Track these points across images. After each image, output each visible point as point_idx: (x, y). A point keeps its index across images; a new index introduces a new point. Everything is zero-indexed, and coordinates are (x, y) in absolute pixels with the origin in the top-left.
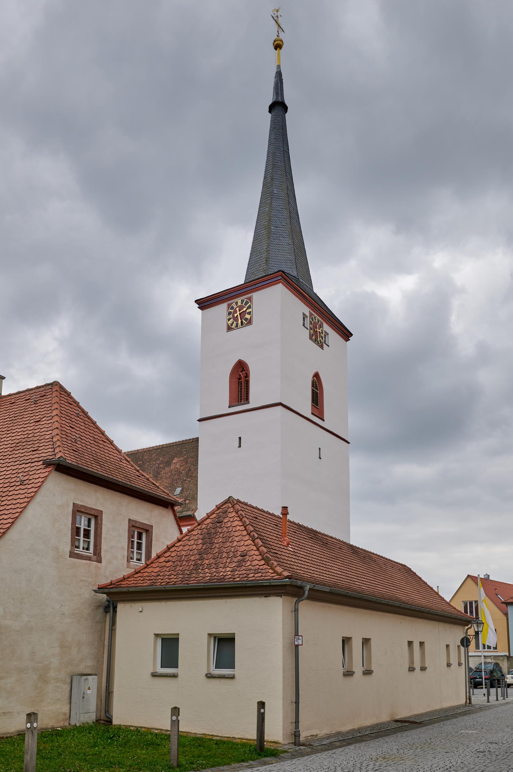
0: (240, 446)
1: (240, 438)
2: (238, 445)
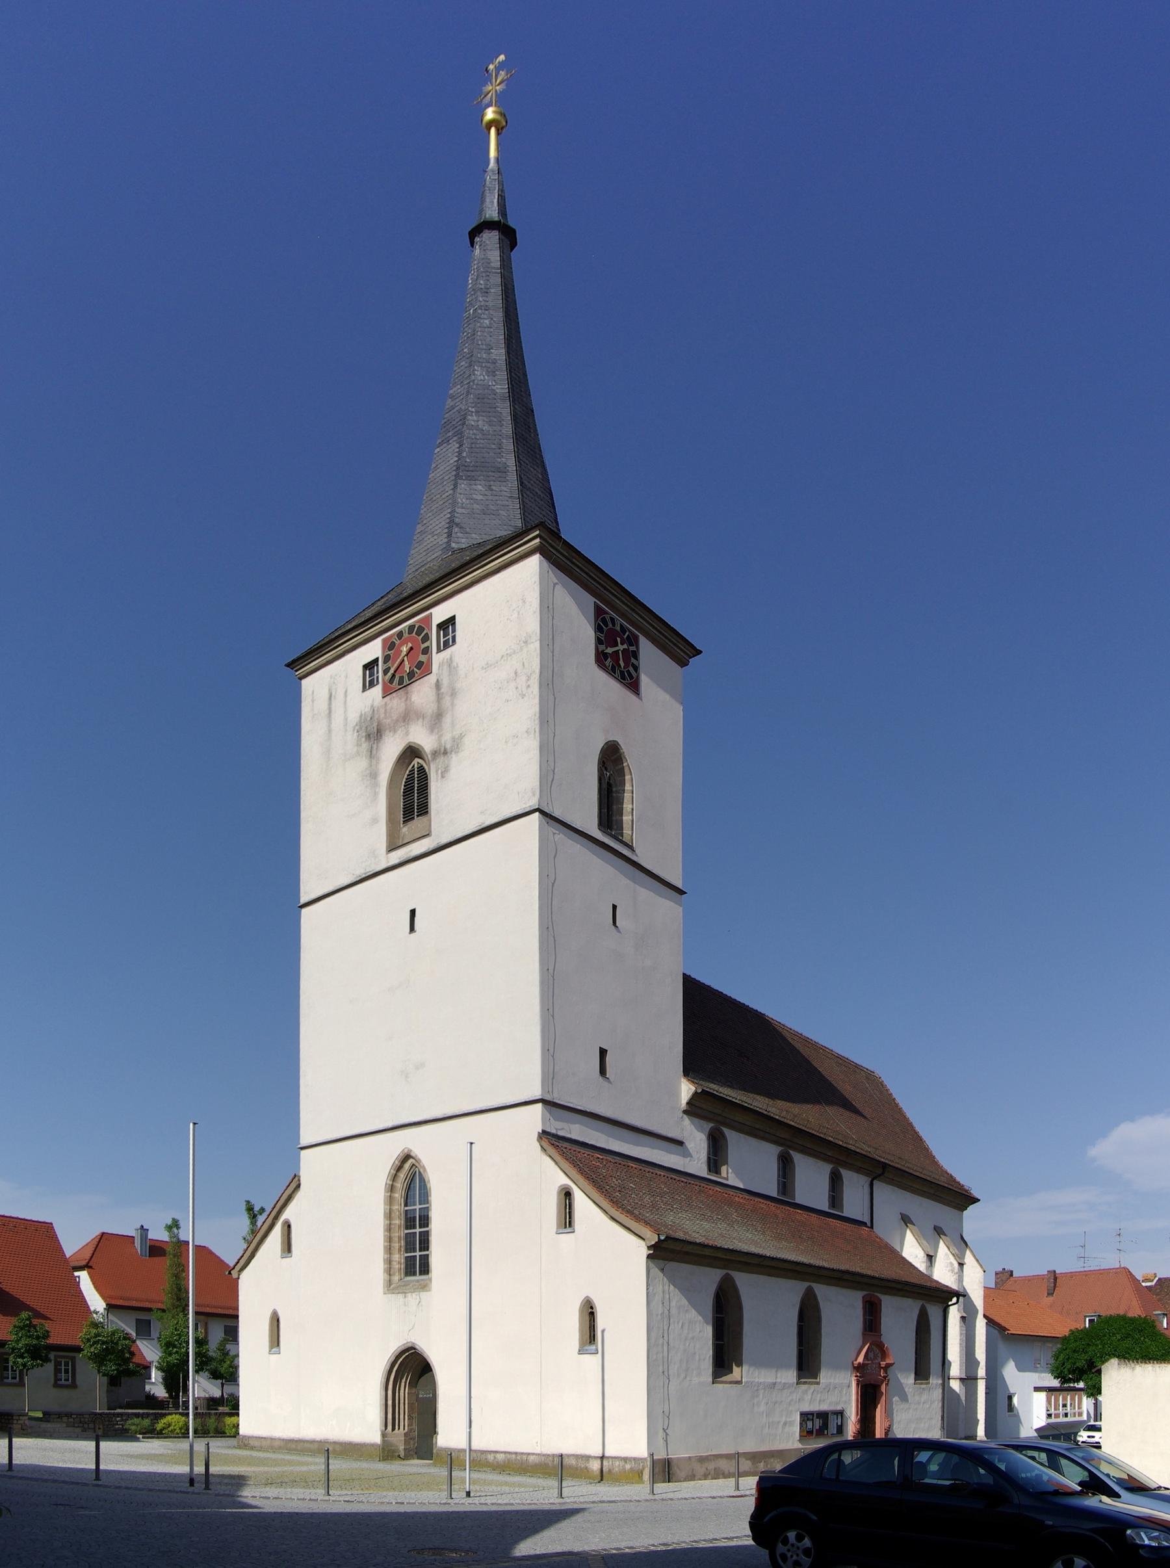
0: (413, 913)
1: (413, 913)
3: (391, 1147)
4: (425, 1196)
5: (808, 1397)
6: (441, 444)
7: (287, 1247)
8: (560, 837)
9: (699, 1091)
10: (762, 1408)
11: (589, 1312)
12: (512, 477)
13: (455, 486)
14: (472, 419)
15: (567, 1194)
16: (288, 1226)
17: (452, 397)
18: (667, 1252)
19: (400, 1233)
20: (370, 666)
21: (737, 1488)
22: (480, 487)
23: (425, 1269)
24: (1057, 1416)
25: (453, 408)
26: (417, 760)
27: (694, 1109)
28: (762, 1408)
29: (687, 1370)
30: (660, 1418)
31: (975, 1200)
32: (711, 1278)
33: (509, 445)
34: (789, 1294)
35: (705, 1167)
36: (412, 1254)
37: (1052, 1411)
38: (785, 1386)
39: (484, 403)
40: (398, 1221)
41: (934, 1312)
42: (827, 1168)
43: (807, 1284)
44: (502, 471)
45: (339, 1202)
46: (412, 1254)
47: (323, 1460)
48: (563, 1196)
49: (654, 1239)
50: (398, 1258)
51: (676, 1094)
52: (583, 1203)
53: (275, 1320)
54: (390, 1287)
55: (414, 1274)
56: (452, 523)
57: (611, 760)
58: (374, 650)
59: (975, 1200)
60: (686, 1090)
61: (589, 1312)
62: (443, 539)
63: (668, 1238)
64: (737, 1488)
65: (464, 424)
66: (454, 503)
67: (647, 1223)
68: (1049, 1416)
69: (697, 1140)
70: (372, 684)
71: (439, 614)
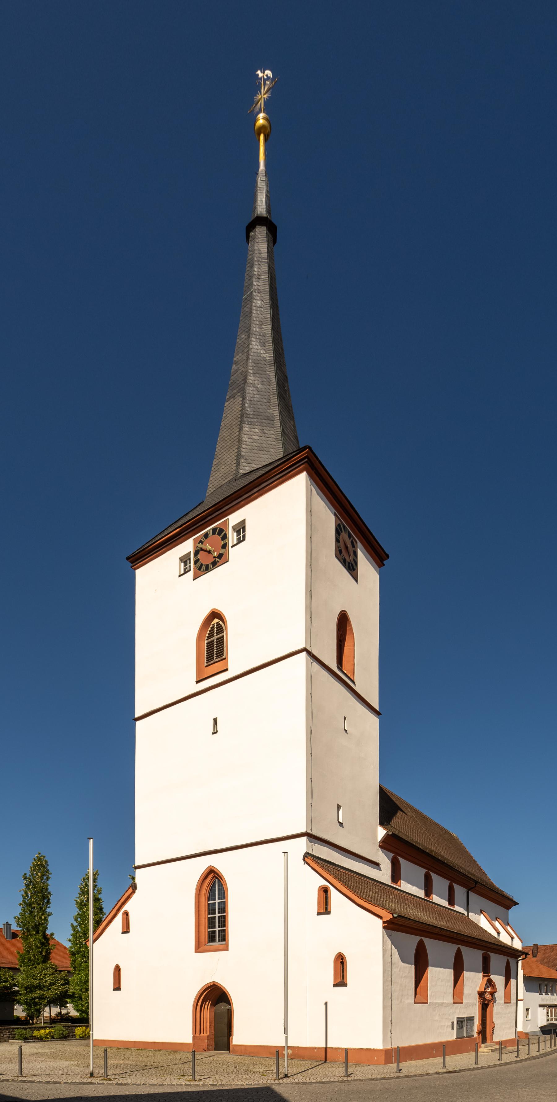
0: (215, 721)
1: (215, 721)
2: (212, 731)
3: (203, 864)
4: (223, 893)
5: (458, 1011)
6: (229, 399)
7: (126, 931)
8: (316, 666)
9: (390, 833)
10: (437, 1017)
11: (340, 961)
12: (278, 423)
13: (241, 429)
14: (251, 378)
15: (325, 890)
16: (126, 914)
17: (236, 363)
18: (395, 926)
19: (205, 916)
20: (185, 560)
21: (444, 1066)
22: (257, 430)
23: (223, 937)
24: (552, 1020)
25: (237, 371)
26: (216, 620)
27: (386, 844)
28: (437, 1017)
29: (402, 995)
30: (389, 1024)
31: (516, 904)
32: (412, 941)
33: (275, 400)
34: (450, 949)
35: (390, 879)
36: (213, 929)
37: (550, 1017)
38: (448, 1005)
39: (259, 371)
40: (204, 910)
41: (512, 961)
42: (447, 883)
43: (458, 946)
44: (270, 419)
45: (161, 904)
46: (213, 929)
47: (273, 1061)
48: (322, 893)
49: (388, 917)
50: (205, 931)
51: (375, 834)
52: (335, 895)
53: (118, 970)
54: (199, 948)
55: (215, 941)
56: (239, 456)
57: (343, 621)
58: (187, 547)
59: (516, 904)
60: (381, 832)
61: (340, 961)
62: (234, 467)
63: (399, 916)
64: (444, 1066)
65: (246, 382)
66: (240, 441)
67: (383, 907)
68: (548, 1020)
69: (385, 861)
70: (185, 572)
71: (234, 519)
